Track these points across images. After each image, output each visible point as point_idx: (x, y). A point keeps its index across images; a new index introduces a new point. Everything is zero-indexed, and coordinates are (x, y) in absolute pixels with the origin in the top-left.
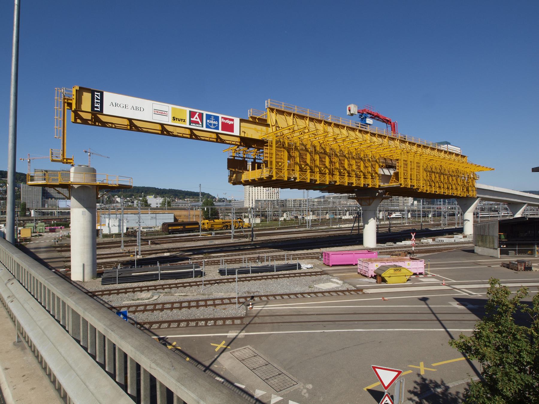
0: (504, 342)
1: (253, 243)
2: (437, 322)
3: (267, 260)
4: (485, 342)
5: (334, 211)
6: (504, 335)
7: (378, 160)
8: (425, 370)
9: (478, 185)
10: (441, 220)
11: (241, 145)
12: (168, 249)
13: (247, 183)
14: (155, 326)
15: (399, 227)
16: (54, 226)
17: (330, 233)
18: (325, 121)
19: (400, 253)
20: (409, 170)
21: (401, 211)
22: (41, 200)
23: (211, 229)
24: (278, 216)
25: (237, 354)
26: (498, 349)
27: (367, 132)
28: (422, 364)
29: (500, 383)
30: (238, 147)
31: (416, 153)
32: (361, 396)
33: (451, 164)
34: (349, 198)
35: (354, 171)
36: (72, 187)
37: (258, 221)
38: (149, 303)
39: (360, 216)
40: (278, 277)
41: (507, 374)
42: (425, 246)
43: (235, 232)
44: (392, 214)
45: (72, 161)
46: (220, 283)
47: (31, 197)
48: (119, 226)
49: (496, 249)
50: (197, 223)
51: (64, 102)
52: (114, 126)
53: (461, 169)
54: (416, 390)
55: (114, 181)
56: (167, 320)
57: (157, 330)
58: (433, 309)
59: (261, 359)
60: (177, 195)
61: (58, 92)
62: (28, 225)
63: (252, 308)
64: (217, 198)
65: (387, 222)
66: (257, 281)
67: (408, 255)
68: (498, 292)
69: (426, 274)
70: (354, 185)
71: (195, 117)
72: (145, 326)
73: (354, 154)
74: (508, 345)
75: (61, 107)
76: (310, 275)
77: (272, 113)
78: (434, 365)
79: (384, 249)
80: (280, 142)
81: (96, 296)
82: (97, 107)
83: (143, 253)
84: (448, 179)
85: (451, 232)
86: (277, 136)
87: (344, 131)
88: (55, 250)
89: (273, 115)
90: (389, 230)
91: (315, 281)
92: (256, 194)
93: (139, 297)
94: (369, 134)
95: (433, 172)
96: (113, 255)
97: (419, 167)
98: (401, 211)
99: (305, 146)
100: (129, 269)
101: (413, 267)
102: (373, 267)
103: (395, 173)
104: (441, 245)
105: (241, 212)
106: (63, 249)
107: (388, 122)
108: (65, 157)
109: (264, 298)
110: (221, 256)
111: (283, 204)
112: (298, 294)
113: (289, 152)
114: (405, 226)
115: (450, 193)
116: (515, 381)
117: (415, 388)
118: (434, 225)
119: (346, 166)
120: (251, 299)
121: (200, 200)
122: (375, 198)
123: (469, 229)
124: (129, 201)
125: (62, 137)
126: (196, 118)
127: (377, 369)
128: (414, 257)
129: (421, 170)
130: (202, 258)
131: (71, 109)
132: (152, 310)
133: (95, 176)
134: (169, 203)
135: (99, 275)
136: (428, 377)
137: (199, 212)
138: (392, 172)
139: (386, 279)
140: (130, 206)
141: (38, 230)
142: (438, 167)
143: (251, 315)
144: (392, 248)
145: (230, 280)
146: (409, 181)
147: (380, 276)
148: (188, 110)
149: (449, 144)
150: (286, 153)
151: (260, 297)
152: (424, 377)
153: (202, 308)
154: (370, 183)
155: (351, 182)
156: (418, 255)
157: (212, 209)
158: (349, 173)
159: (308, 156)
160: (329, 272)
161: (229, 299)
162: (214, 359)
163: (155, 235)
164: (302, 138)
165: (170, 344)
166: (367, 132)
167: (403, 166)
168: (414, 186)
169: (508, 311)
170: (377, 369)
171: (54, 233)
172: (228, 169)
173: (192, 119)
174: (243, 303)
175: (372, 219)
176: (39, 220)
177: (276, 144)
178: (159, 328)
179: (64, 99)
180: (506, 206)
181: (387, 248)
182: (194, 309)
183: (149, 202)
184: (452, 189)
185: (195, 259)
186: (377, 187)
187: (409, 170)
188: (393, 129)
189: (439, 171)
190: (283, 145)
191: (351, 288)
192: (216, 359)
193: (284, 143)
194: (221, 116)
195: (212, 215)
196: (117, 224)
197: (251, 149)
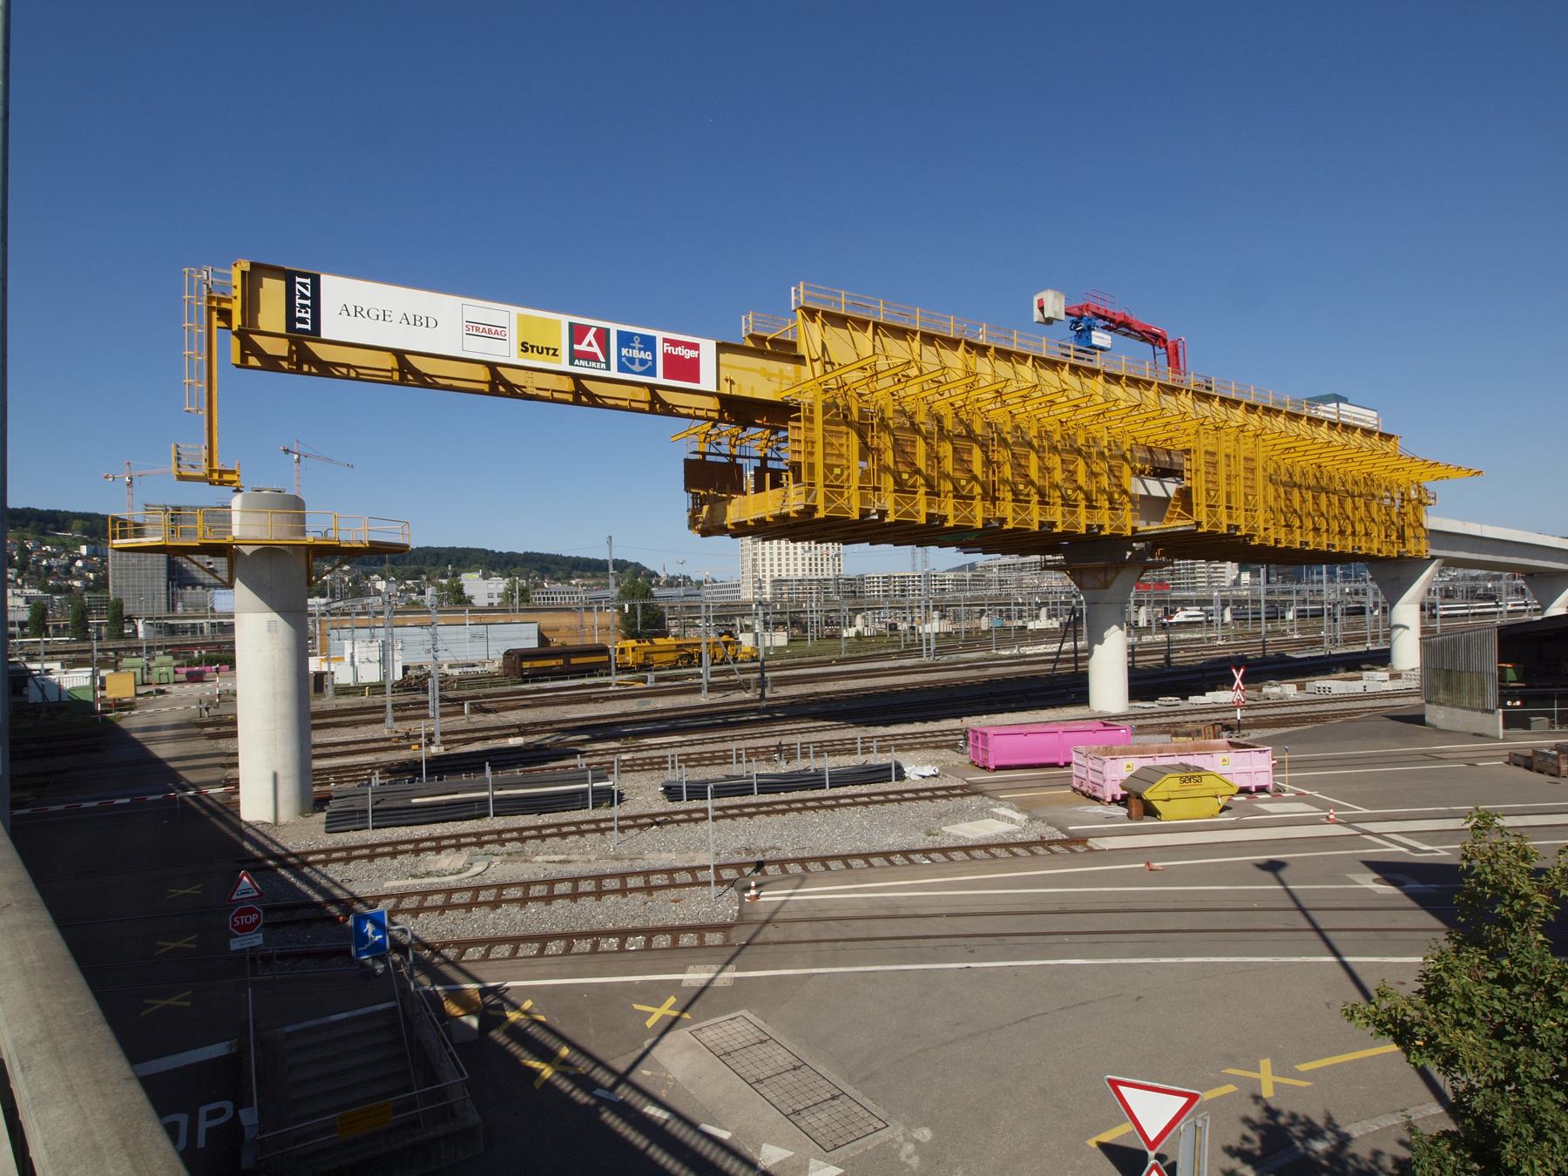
0: (1520, 1014)
1: (764, 704)
2: (1314, 935)
3: (805, 755)
4: (1457, 1012)
5: (1003, 606)
6: (1517, 989)
7: (1128, 455)
9: (1433, 521)
10: (1322, 628)
12: (518, 726)
13: (741, 530)
14: (474, 953)
15: (1197, 650)
16: (199, 664)
17: (991, 671)
18: (967, 343)
19: (1200, 726)
21: (1201, 603)
25: (709, 1035)
27: (1094, 373)
28: (1265, 1064)
29: (1509, 1147)
30: (714, 426)
31: (1242, 429)
32: (1078, 1162)
33: (1348, 461)
34: (1046, 567)
35: (1057, 487)
36: (238, 551)
37: (781, 639)
38: (459, 885)
39: (1078, 621)
40: (836, 803)
41: (1530, 1116)
42: (1275, 706)
43: (713, 674)
45: (234, 477)
46: (666, 823)
47: (139, 587)
49: (1492, 712)
50: (603, 650)
51: (210, 309)
52: (352, 374)
53: (1379, 473)
54: (1247, 1146)
55: (355, 533)
56: (511, 934)
58: (1300, 898)
59: (781, 1050)
61: (191, 279)
62: (126, 662)
63: (757, 896)
64: (663, 575)
65: (1162, 637)
66: (774, 817)
67: (1225, 734)
68: (1496, 856)
69: (1279, 790)
70: (1059, 529)
72: (446, 951)
73: (1057, 437)
74: (1530, 1023)
77: (810, 324)
78: (1303, 1067)
79: (1152, 716)
80: (837, 407)
81: (309, 864)
82: (303, 321)
83: (448, 737)
84: (1342, 506)
86: (826, 391)
87: (1026, 371)
88: (198, 735)
89: (815, 328)
90: (1168, 659)
92: (776, 562)
93: (432, 868)
94: (1100, 378)
95: (1295, 485)
96: (362, 746)
97: (1252, 470)
98: (1201, 603)
99: (911, 418)
100: (405, 785)
101: (1239, 769)
102: (1117, 772)
103: (1179, 491)
104: (1322, 702)
105: (728, 616)
106: (223, 729)
107: (1156, 339)
109: (794, 868)
110: (671, 745)
111: (853, 589)
112: (894, 853)
113: (862, 436)
114: (1214, 648)
115: (1349, 545)
116: (1557, 1139)
117: (1245, 1138)
118: (1301, 644)
119: (1034, 474)
120: (756, 871)
122: (1123, 565)
123: (1408, 652)
124: (412, 590)
125: (205, 409)
126: (590, 344)
127: (1122, 1089)
128: (1242, 741)
130: (617, 751)
131: (230, 328)
132: (468, 907)
133: (302, 519)
134: (524, 593)
135: (320, 803)
136: (1286, 1106)
137: (610, 617)
138: (1172, 487)
139: (1158, 805)
140: (415, 603)
141: (154, 677)
142: (1311, 471)
143: (755, 917)
144: (1175, 714)
145: (695, 815)
146: (1222, 512)
147: (1139, 797)
148: (565, 320)
149: (1345, 401)
150: (854, 439)
151: (782, 863)
152: (1273, 1105)
153: (610, 900)
154: (1105, 521)
155: (1049, 519)
156: (1255, 734)
157: (644, 606)
158: (1041, 493)
159: (921, 447)
160: (987, 787)
161: (692, 870)
162: (640, 1052)
163: (483, 685)
164: (902, 393)
165: (516, 1007)
166: (1094, 373)
167: (1203, 469)
168: (1237, 528)
169: (1529, 914)
170: (1122, 1089)
171: (198, 686)
172: (687, 489)
173: (576, 347)
175: (1115, 627)
176: (159, 648)
177: (824, 414)
178: (485, 958)
179: (210, 299)
180: (1520, 582)
181: (1160, 715)
182: (588, 902)
183: (467, 591)
184: (1354, 533)
185: (595, 753)
186: (1129, 533)
188: (1174, 359)
189: (1312, 482)
190: (845, 416)
191: (1054, 833)
192: (647, 1052)
193: (849, 409)
194: (660, 335)
195: (645, 624)
196: (375, 655)
197: (752, 431)
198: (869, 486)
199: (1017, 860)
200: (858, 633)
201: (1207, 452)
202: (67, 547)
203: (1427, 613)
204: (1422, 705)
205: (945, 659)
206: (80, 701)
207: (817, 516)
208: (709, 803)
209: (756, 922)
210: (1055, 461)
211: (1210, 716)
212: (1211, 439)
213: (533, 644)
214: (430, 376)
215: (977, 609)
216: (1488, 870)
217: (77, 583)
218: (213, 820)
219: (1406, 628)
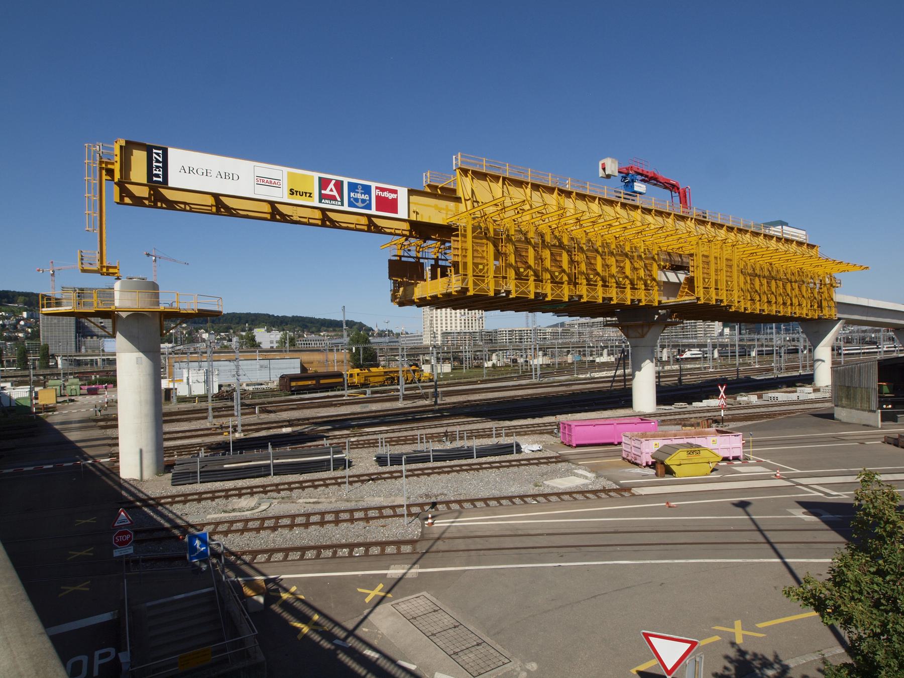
0: (890, 593)
1: (437, 407)
2: (767, 546)
3: (461, 438)
4: (852, 592)
5: (581, 349)
6: (888, 578)
7: (656, 257)
8: (744, 636)
9: (839, 297)
11: (411, 236)
12: (288, 421)
14: (261, 558)
16: (95, 383)
18: (559, 190)
19: (699, 421)
20: (713, 273)
21: (700, 346)
22: (74, 340)
23: (365, 385)
24: (482, 359)
25: (403, 607)
26: (877, 604)
27: (636, 207)
28: (738, 623)
30: (406, 240)
31: (724, 241)
33: (789, 261)
34: (606, 325)
35: (613, 276)
36: (118, 315)
38: (253, 517)
40: (480, 467)
42: (744, 408)
43: (406, 389)
44: (684, 352)
45: (116, 271)
46: (378, 479)
47: (58, 337)
48: (207, 382)
49: (874, 412)
50: (340, 375)
51: (101, 169)
52: (188, 208)
53: (807, 268)
54: (727, 673)
56: (284, 546)
57: (264, 565)
59: (447, 616)
60: (306, 327)
62: (51, 382)
63: (432, 523)
64: (376, 329)
65: (676, 367)
67: (714, 425)
68: (876, 498)
69: (747, 459)
70: (614, 302)
71: (329, 188)
73: (613, 246)
75: (95, 176)
76: (537, 464)
77: (464, 178)
78: (760, 625)
80: (481, 228)
81: (161, 505)
83: (246, 428)
84: (784, 288)
85: (791, 383)
86: (474, 219)
87: (595, 206)
89: (467, 181)
90: (680, 380)
91: (546, 474)
92: (444, 322)
94: (639, 211)
95: (756, 275)
97: (731, 267)
98: (700, 346)
99: (525, 234)
100: (220, 456)
101: (722, 446)
102: (649, 448)
103: (687, 279)
105: (415, 355)
106: (109, 423)
107: (673, 187)
108: (105, 264)
109: (455, 506)
110: (381, 432)
111: (491, 338)
112: (515, 497)
113: (496, 246)
114: (708, 373)
115: (788, 311)
117: (726, 668)
118: (760, 371)
119: (599, 269)
120: (432, 508)
121: (345, 334)
122: (651, 324)
123: (824, 376)
124: (224, 339)
125: (98, 229)
126: (331, 190)
127: (651, 638)
128: (724, 429)
129: (735, 273)
130: (348, 436)
131: (113, 180)
132: (258, 530)
133: (157, 296)
134: (292, 340)
135: (168, 468)
136: (751, 649)
137: (344, 355)
138: (682, 277)
139: (674, 468)
140: (226, 347)
141: (68, 392)
142: (766, 266)
143: (431, 536)
146: (713, 292)
147: (662, 463)
148: (316, 175)
149: (787, 224)
150: (491, 247)
151: (447, 503)
152: (743, 648)
154: (642, 296)
155: (609, 296)
156: (732, 425)
157: (365, 349)
158: (604, 280)
159: (531, 253)
161: (393, 508)
163: (266, 396)
164: (520, 220)
166: (636, 207)
167: (701, 266)
168: (721, 301)
169: (895, 533)
170: (651, 638)
171: (94, 397)
172: (390, 278)
173: (323, 192)
174: (417, 515)
175: (648, 361)
176: (71, 374)
177: (473, 232)
178: (268, 561)
179: (101, 163)
180: (891, 334)
181: (675, 414)
183: (258, 339)
184: (791, 304)
185: (335, 437)
187: (713, 273)
188: (684, 199)
189: (767, 274)
190: (486, 234)
192: (366, 617)
193: (488, 229)
194: (373, 185)
195: (365, 359)
196: (202, 378)
197: (429, 242)
198: (500, 275)
199: (589, 501)
200: (494, 364)
201: (703, 256)
202: (15, 313)
203: (835, 352)
204: (832, 408)
205: (546, 380)
206: (23, 406)
207: (469, 294)
208: (403, 467)
209: (432, 539)
210: (612, 261)
211: (705, 414)
212: (706, 248)
213: (298, 371)
214: (338, 222)
215: (566, 350)
216: (871, 506)
217: (21, 335)
218: (104, 478)
219: (823, 361)
